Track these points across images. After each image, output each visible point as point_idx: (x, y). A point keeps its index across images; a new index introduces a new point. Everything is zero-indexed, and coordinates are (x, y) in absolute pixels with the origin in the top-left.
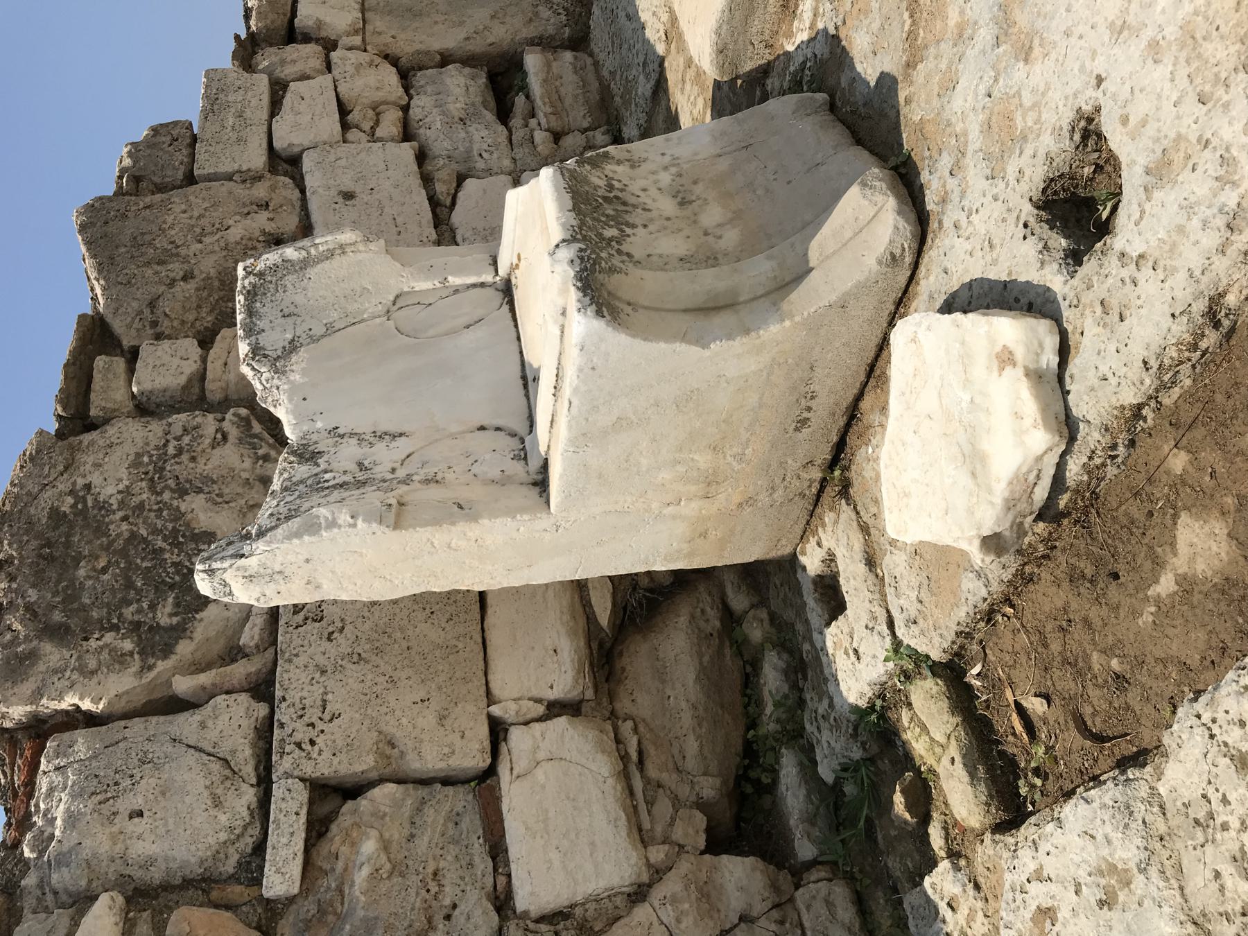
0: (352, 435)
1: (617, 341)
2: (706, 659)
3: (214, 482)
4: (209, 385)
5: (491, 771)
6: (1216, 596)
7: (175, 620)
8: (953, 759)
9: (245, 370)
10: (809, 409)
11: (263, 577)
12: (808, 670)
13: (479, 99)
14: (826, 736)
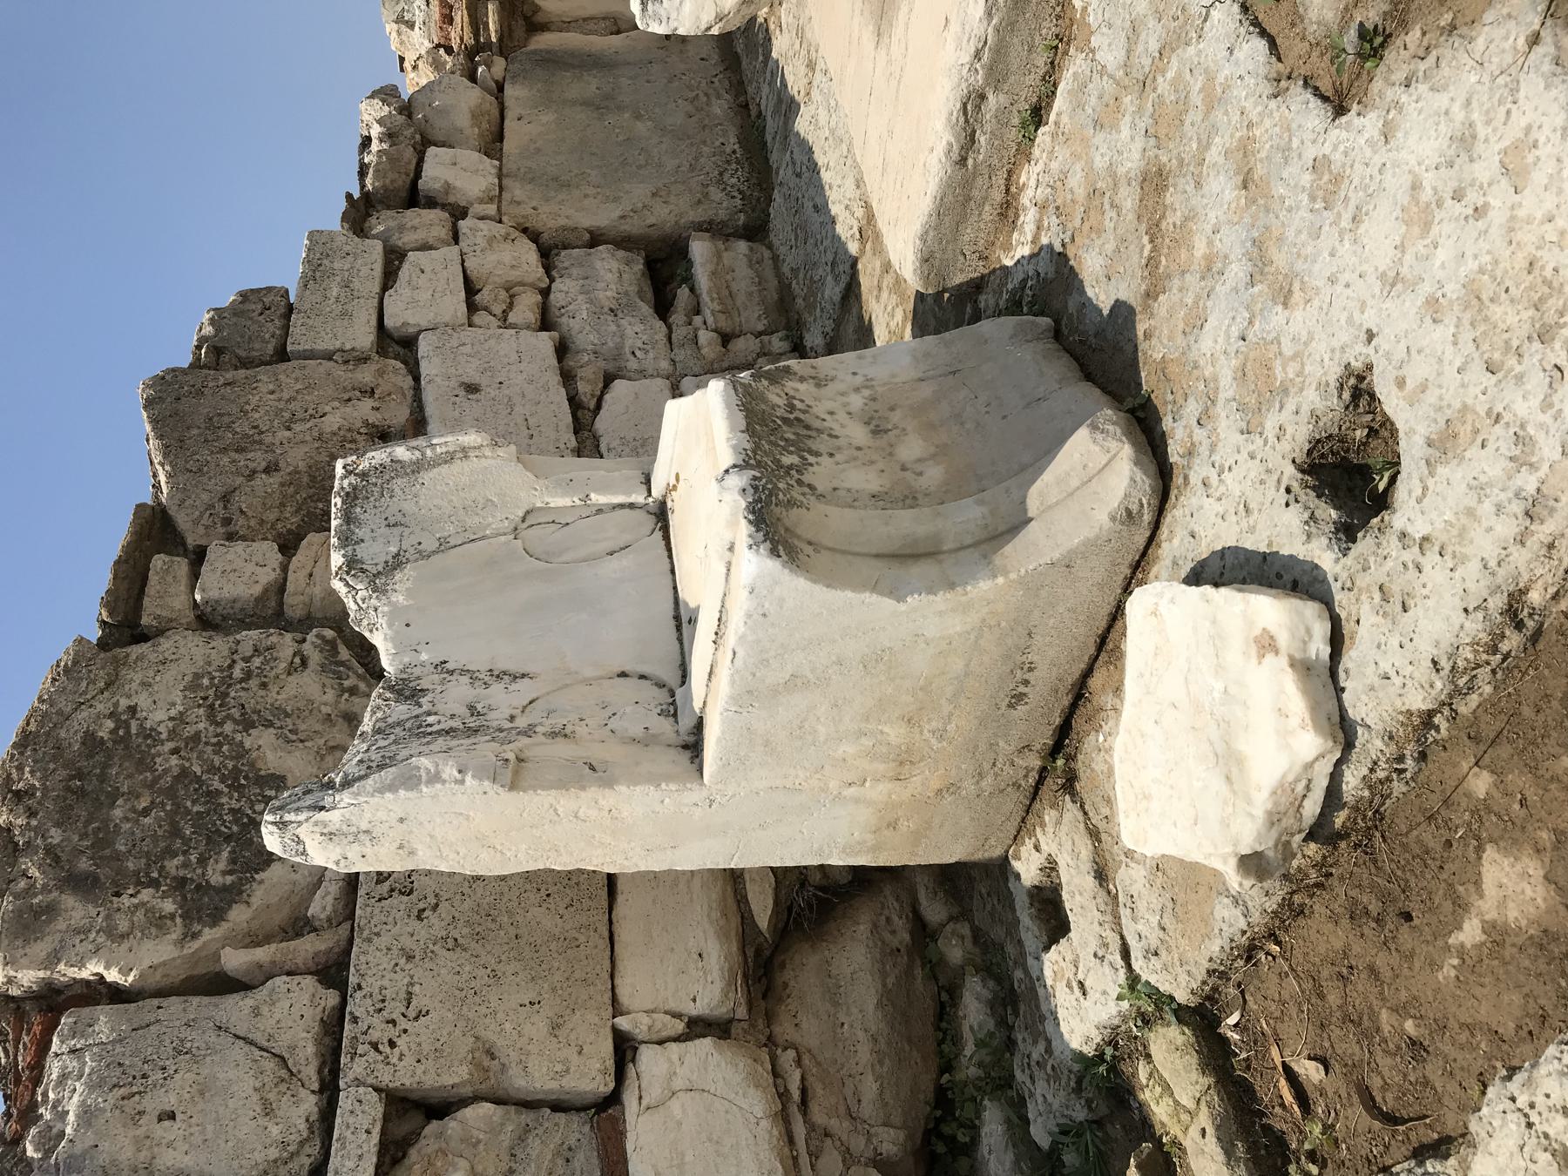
0: (464, 672)
1: (795, 587)
2: (890, 981)
3: (287, 715)
4: (288, 599)
5: (614, 1099)
6: (1532, 951)
7: (229, 879)
8: (1204, 1130)
9: (337, 585)
10: (1026, 683)
11: (346, 835)
12: (1021, 1004)
13: (633, 289)
14: (1041, 1088)
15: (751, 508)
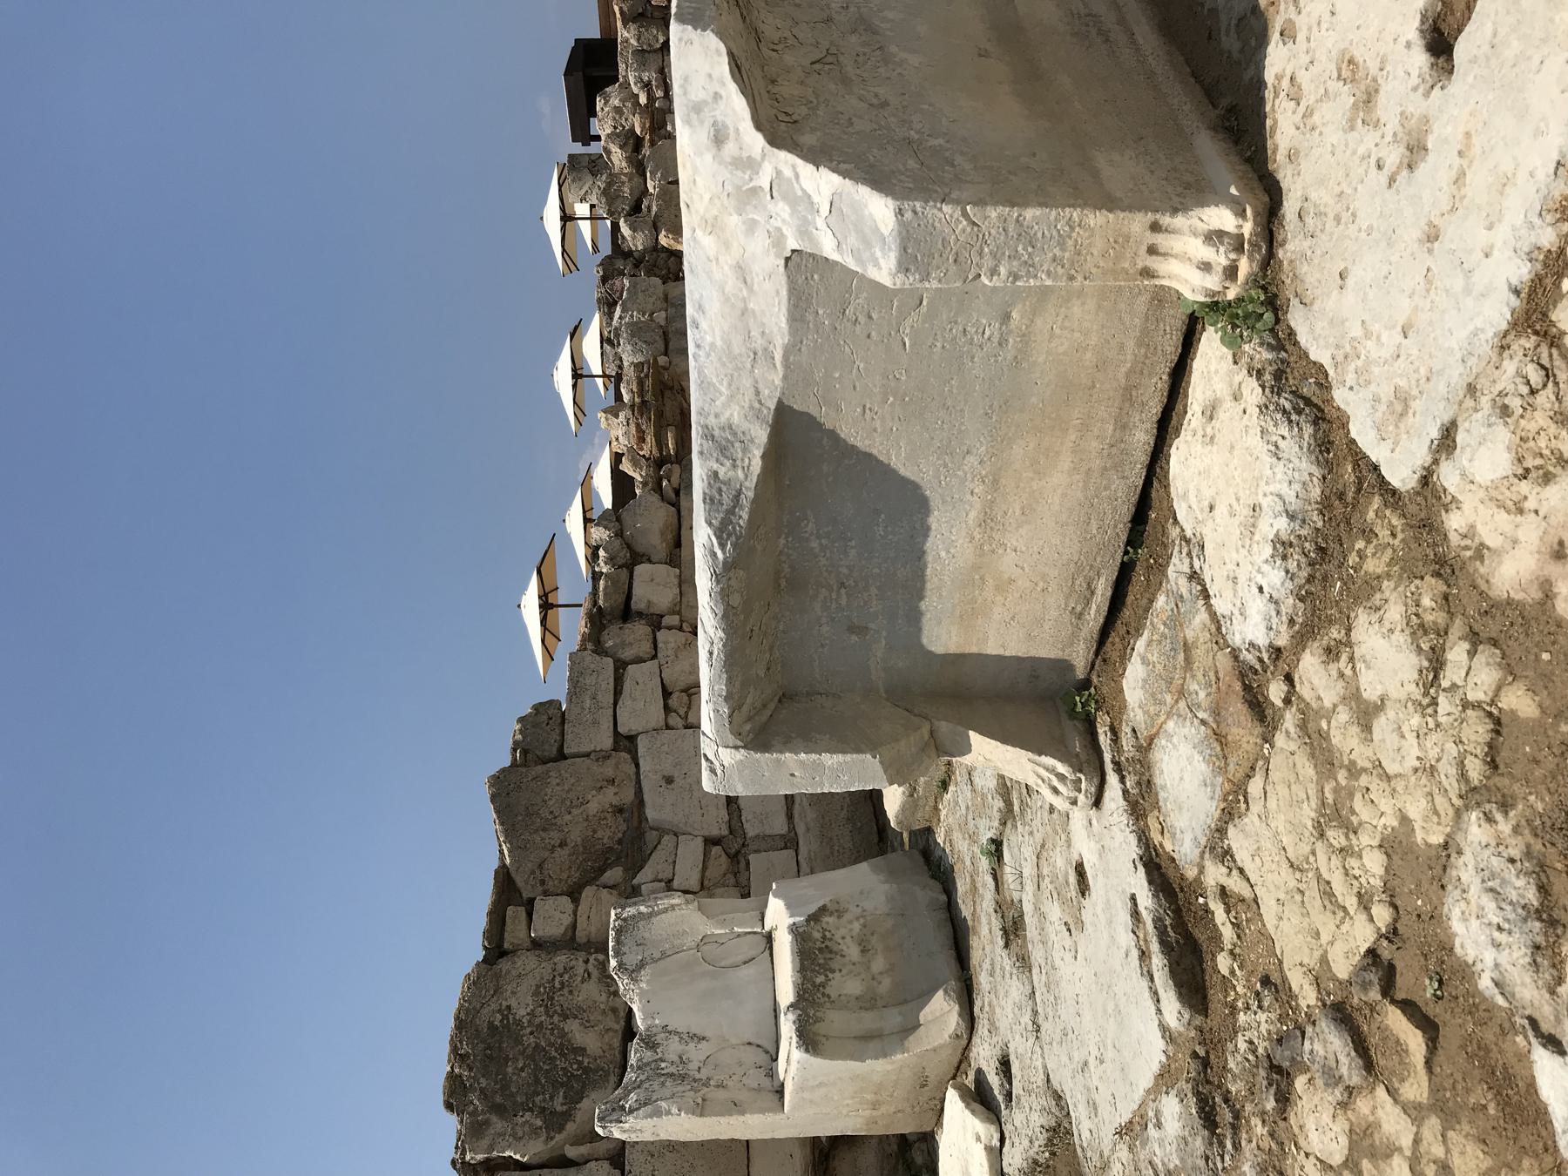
15: (797, 1030)
